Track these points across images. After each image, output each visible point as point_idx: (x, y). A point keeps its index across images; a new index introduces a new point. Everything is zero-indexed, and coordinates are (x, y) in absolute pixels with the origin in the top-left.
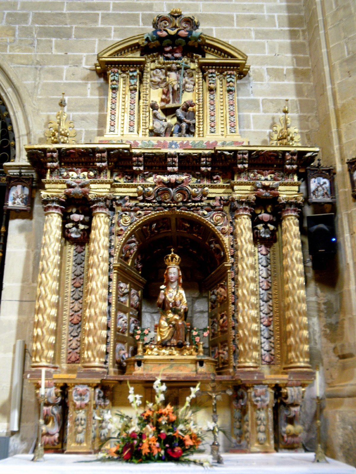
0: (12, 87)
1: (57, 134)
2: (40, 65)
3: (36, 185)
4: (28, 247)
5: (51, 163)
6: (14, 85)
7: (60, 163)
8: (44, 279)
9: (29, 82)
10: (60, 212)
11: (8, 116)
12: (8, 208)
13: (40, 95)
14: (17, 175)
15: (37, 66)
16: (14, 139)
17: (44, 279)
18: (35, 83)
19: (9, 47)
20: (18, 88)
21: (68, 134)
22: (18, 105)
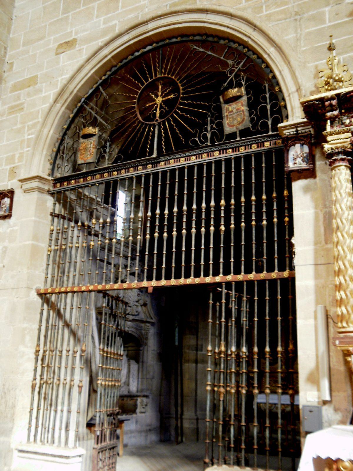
0: (273, 46)
1: (331, 81)
2: (300, 15)
3: (315, 139)
4: (316, 207)
5: (331, 113)
6: (275, 44)
7: (340, 111)
8: (341, 238)
9: (291, 36)
10: (347, 164)
11: (274, 77)
12: (290, 169)
13: (304, 46)
14: (294, 134)
15: (296, 17)
16: (284, 99)
17: (341, 238)
18: (297, 36)
19: (264, 7)
20: (280, 45)
21: (343, 79)
22: (283, 63)
